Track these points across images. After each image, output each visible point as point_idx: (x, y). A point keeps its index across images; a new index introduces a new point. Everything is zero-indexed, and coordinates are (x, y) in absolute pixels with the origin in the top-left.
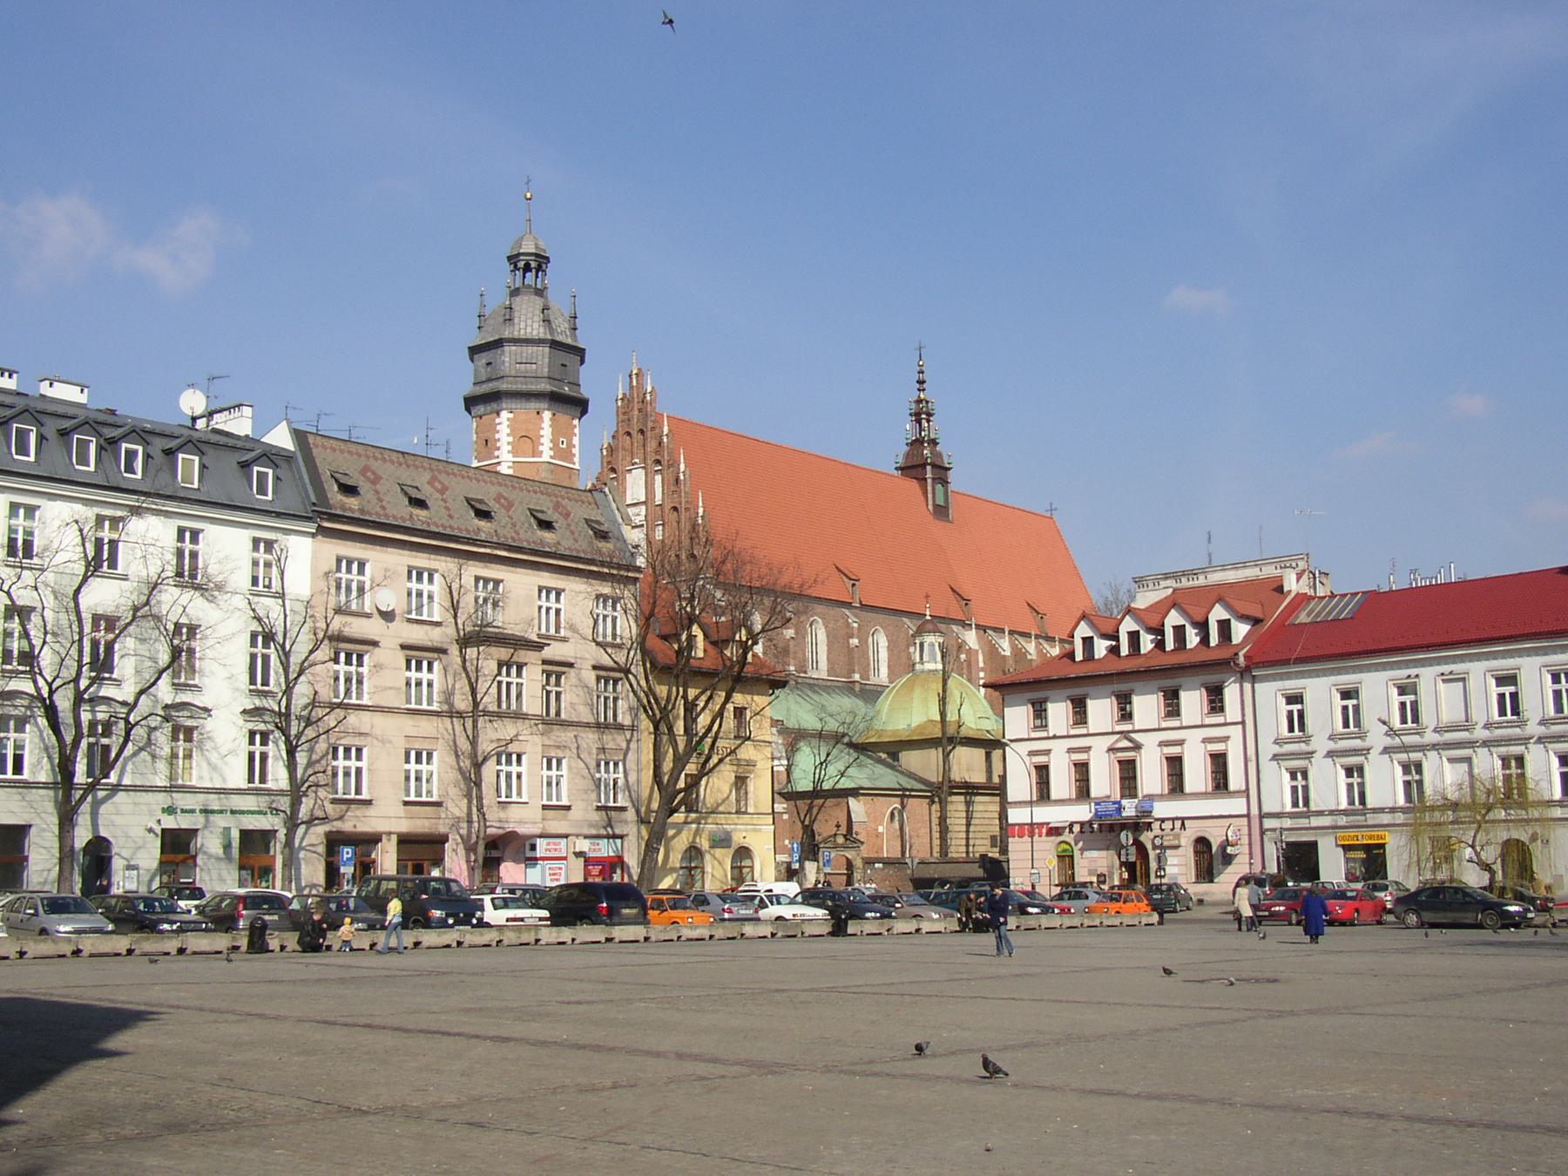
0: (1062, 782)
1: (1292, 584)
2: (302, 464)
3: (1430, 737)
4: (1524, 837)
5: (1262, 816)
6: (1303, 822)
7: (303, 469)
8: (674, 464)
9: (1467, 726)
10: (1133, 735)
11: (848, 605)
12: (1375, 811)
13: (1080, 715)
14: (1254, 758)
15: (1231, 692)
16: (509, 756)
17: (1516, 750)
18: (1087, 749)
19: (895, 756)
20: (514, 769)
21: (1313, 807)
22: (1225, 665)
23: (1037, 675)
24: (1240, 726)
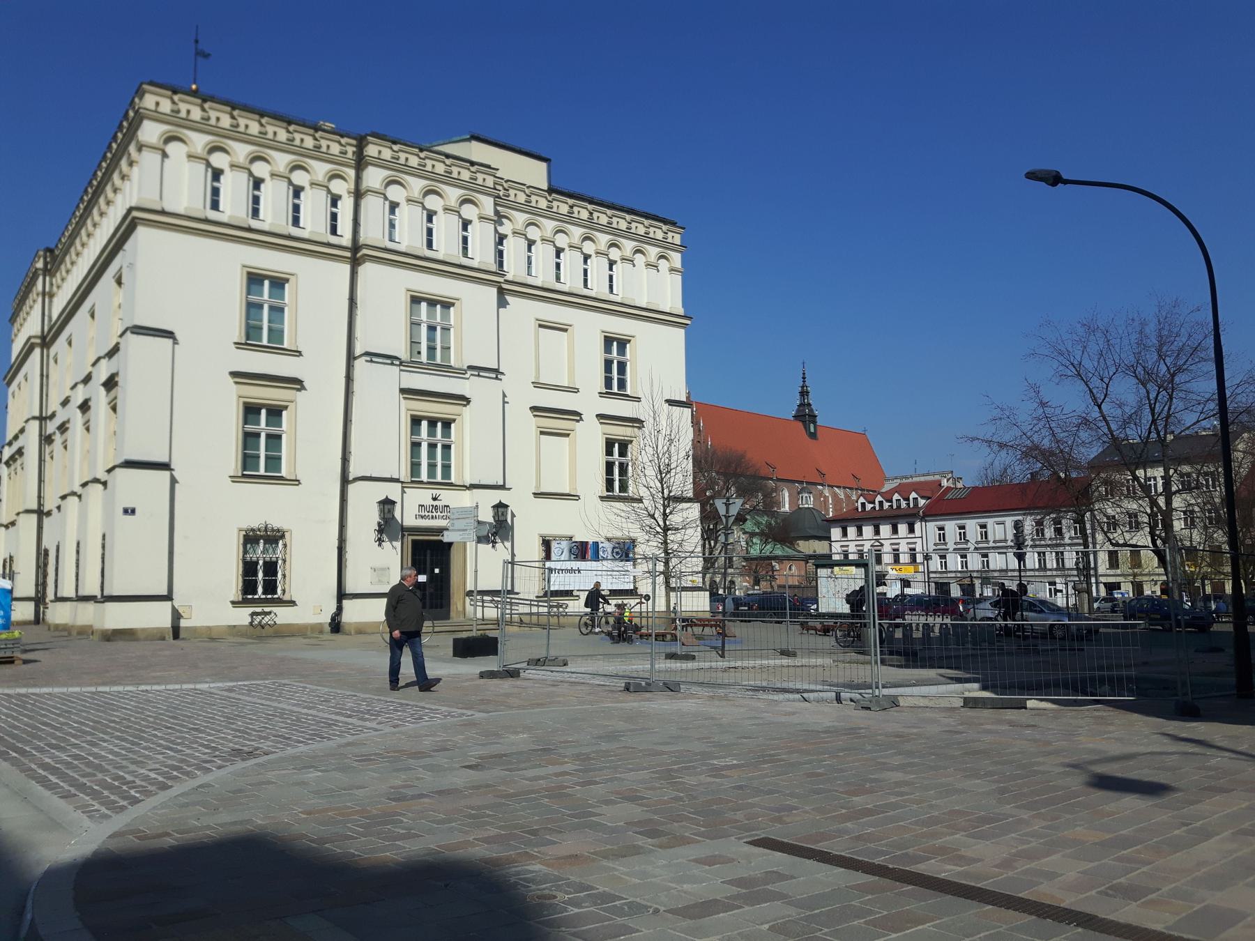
1: (945, 483)
3: (991, 544)
5: (928, 573)
6: (945, 575)
9: (1005, 541)
11: (771, 479)
12: (1068, 569)
13: (860, 533)
15: (917, 526)
23: (844, 517)
24: (350, 588)
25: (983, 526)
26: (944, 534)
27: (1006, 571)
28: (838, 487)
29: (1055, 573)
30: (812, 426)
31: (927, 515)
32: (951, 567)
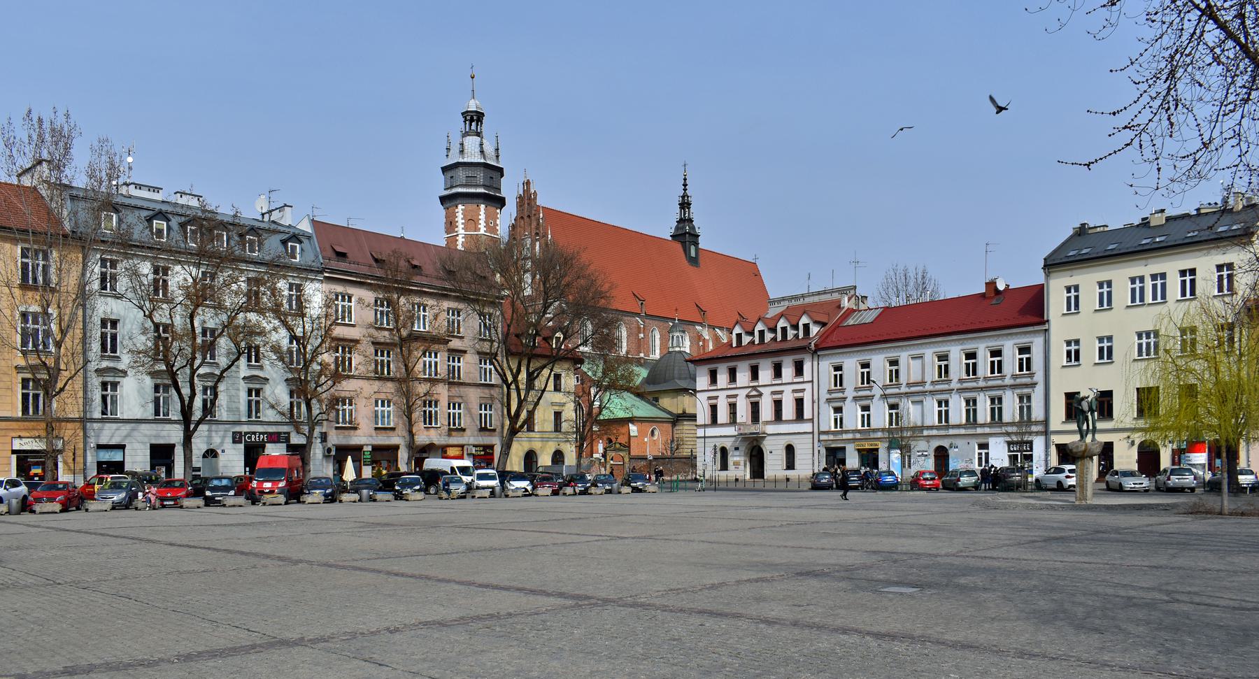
0: (723, 416)
1: (846, 303)
2: (315, 240)
3: (904, 389)
4: (947, 446)
7: (316, 243)
8: (545, 235)
9: (923, 383)
10: (759, 389)
11: (638, 315)
14: (817, 401)
15: (807, 367)
16: (430, 402)
17: (1026, 391)
18: (716, 398)
19: (657, 400)
20: (457, 411)
21: (844, 428)
22: (803, 349)
25: (894, 363)
26: (841, 375)
27: (923, 428)
28: (721, 328)
29: (987, 430)
30: (693, 248)
31: (818, 350)
32: (848, 425)
